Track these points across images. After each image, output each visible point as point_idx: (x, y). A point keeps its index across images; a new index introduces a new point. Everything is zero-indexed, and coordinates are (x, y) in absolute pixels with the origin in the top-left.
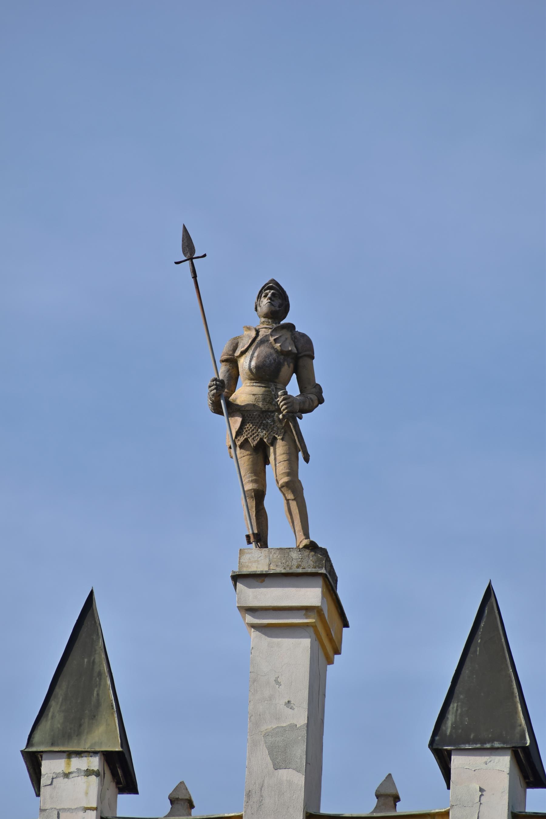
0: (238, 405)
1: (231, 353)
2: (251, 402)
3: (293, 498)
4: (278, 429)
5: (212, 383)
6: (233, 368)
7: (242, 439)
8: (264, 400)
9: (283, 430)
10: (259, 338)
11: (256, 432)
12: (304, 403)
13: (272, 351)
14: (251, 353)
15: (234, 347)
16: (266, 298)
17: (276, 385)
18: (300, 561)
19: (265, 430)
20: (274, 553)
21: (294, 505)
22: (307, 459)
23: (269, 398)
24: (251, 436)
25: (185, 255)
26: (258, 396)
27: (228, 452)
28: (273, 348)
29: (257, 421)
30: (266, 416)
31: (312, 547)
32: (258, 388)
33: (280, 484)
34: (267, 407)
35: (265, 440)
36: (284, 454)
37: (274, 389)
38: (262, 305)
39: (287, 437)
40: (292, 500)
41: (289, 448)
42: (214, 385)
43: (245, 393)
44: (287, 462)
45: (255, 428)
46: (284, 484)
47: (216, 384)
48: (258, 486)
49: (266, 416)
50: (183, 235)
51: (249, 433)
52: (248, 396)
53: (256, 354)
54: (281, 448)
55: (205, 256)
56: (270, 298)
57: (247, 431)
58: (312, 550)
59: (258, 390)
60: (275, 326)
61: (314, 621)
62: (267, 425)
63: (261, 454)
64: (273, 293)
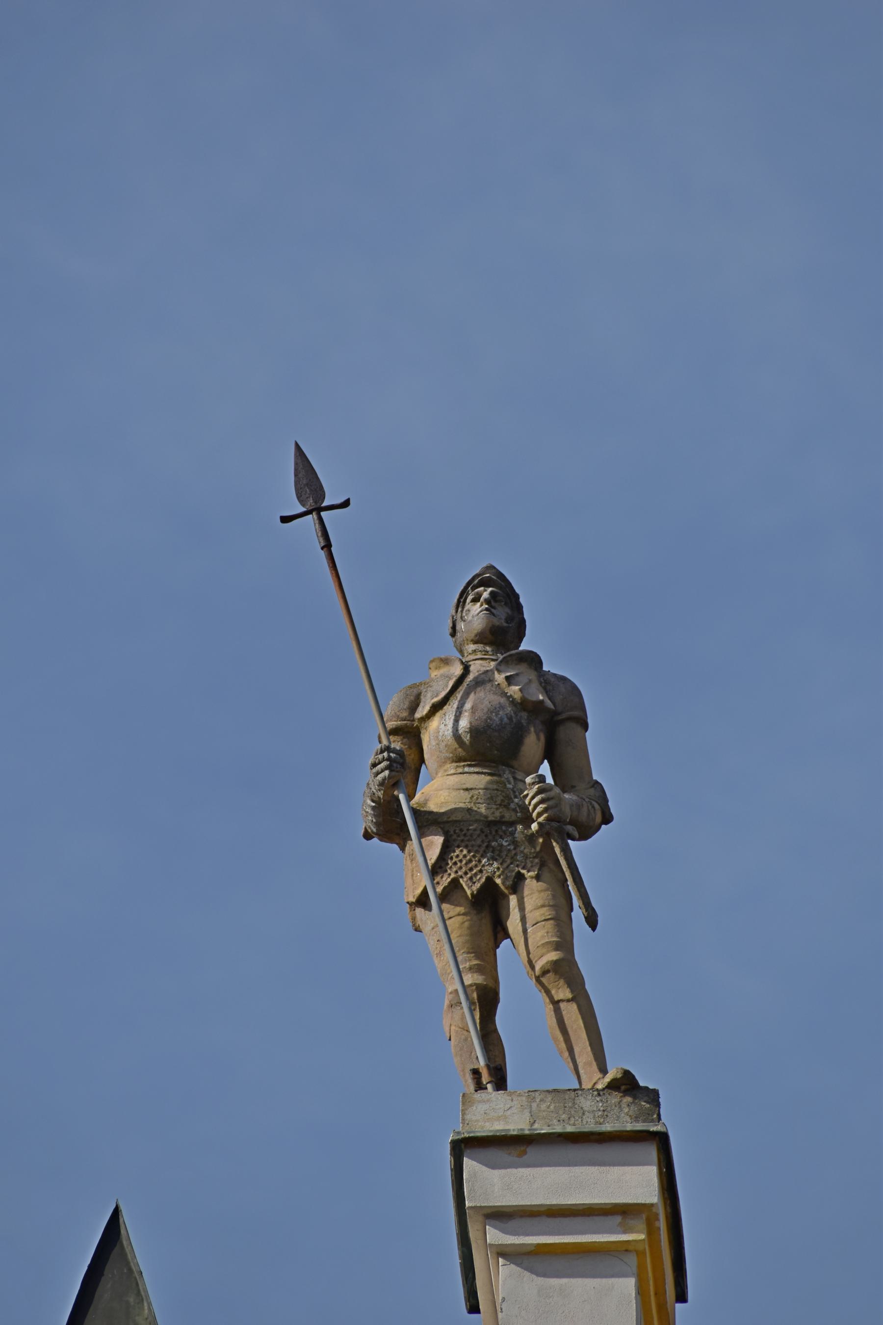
0: (431, 813)
1: (405, 714)
2: (462, 805)
3: (569, 995)
4: (526, 857)
5: (380, 756)
6: (410, 748)
7: (445, 881)
8: (490, 800)
9: (537, 860)
10: (471, 677)
11: (476, 866)
12: (579, 807)
13: (503, 700)
14: (455, 706)
15: (411, 702)
16: (479, 604)
17: (514, 773)
18: (602, 1116)
19: (496, 860)
20: (541, 1101)
21: (571, 1012)
22: (592, 921)
23: (505, 796)
24: (466, 873)
25: (302, 503)
26: (476, 792)
27: (409, 917)
28: (504, 694)
29: (479, 842)
30: (496, 831)
31: (626, 1084)
32: (476, 776)
33: (538, 968)
34: (498, 814)
35: (498, 881)
36: (543, 906)
37: (512, 780)
38: (469, 618)
39: (546, 875)
40: (568, 1001)
41: (554, 896)
42: (384, 760)
43: (443, 787)
44: (552, 922)
45: (474, 856)
46: (548, 967)
47: (389, 759)
48: (485, 980)
49: (496, 831)
50: (296, 464)
51: (461, 868)
52: (454, 793)
53: (468, 706)
54: (536, 895)
55: (346, 504)
56: (487, 601)
57: (455, 863)
58: (626, 1093)
59: (479, 780)
60: (501, 657)
61: (642, 1237)
62: (500, 851)
63: (489, 910)
64: (491, 593)
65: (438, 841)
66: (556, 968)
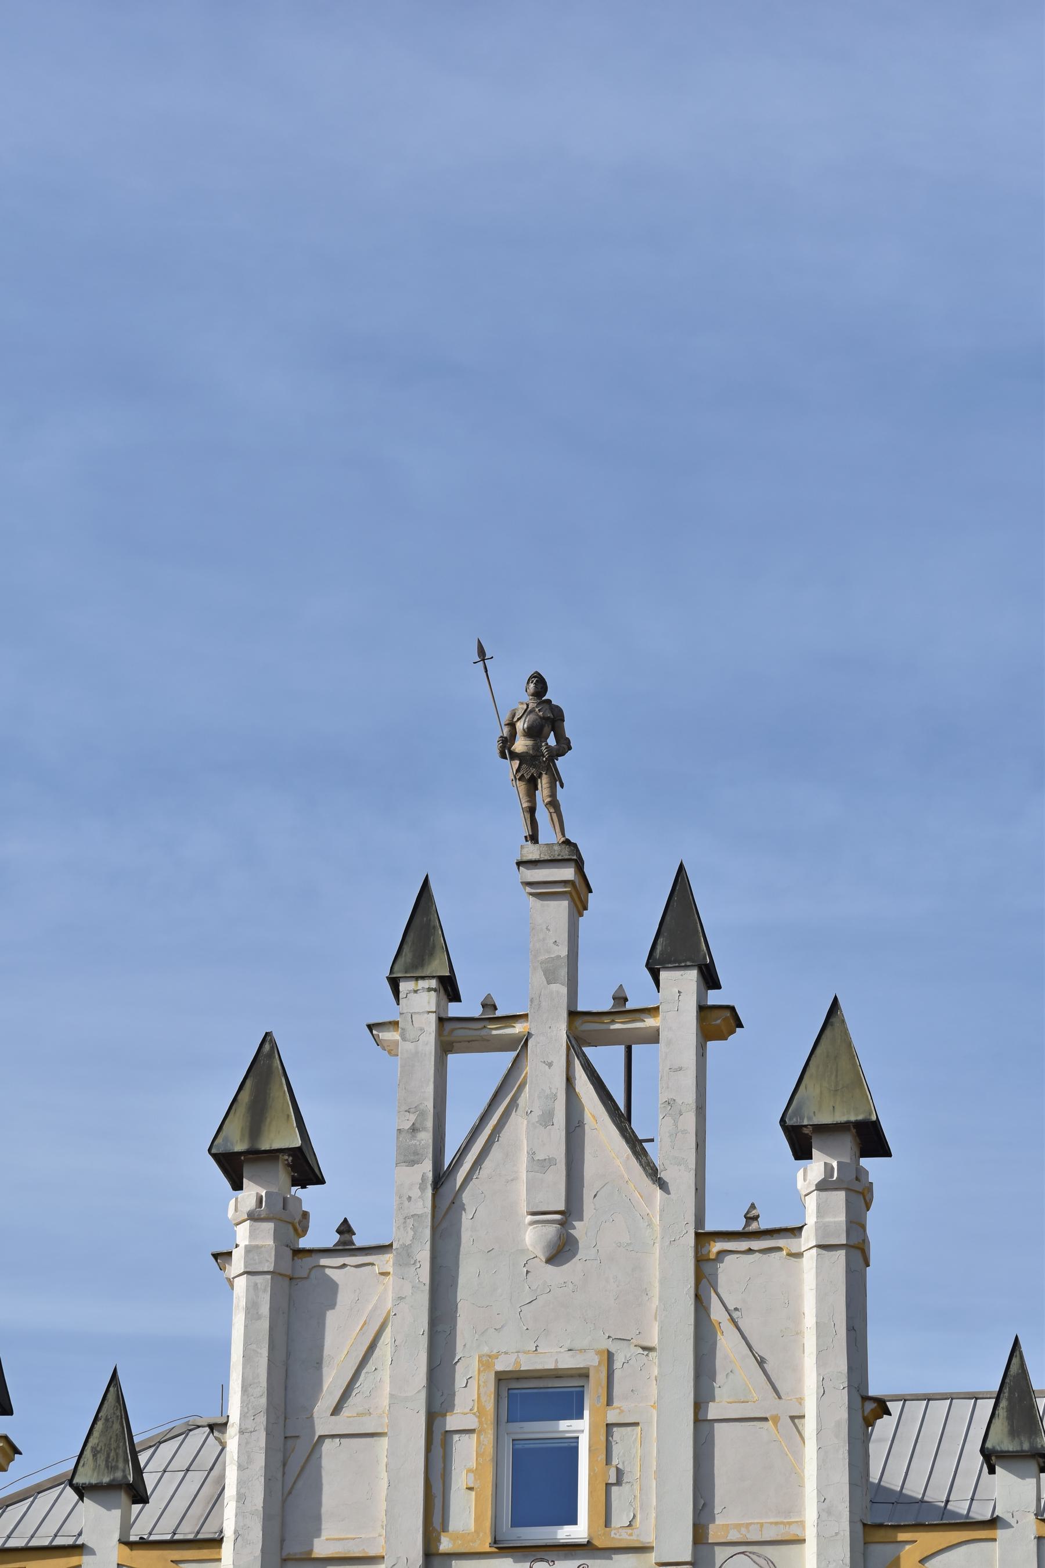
22: (562, 786)
23: (537, 748)
31: (567, 842)
43: (521, 745)
63: (532, 784)
65: (518, 762)
66: (549, 803)
